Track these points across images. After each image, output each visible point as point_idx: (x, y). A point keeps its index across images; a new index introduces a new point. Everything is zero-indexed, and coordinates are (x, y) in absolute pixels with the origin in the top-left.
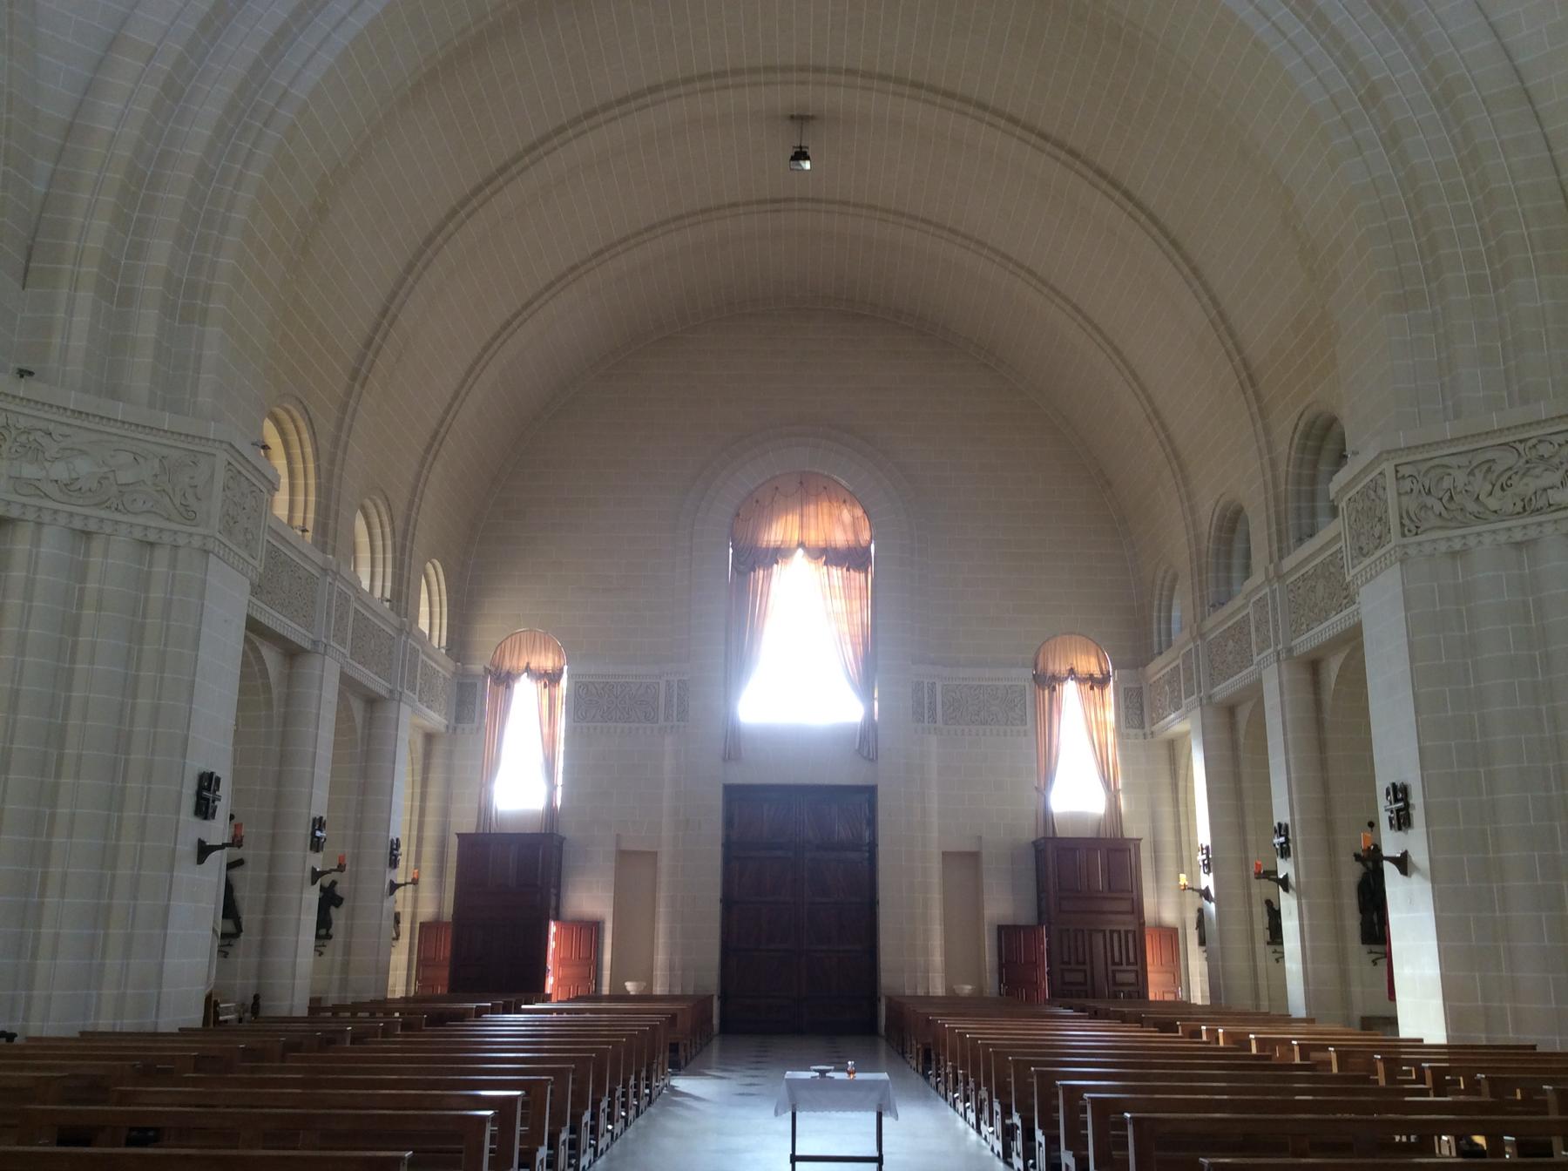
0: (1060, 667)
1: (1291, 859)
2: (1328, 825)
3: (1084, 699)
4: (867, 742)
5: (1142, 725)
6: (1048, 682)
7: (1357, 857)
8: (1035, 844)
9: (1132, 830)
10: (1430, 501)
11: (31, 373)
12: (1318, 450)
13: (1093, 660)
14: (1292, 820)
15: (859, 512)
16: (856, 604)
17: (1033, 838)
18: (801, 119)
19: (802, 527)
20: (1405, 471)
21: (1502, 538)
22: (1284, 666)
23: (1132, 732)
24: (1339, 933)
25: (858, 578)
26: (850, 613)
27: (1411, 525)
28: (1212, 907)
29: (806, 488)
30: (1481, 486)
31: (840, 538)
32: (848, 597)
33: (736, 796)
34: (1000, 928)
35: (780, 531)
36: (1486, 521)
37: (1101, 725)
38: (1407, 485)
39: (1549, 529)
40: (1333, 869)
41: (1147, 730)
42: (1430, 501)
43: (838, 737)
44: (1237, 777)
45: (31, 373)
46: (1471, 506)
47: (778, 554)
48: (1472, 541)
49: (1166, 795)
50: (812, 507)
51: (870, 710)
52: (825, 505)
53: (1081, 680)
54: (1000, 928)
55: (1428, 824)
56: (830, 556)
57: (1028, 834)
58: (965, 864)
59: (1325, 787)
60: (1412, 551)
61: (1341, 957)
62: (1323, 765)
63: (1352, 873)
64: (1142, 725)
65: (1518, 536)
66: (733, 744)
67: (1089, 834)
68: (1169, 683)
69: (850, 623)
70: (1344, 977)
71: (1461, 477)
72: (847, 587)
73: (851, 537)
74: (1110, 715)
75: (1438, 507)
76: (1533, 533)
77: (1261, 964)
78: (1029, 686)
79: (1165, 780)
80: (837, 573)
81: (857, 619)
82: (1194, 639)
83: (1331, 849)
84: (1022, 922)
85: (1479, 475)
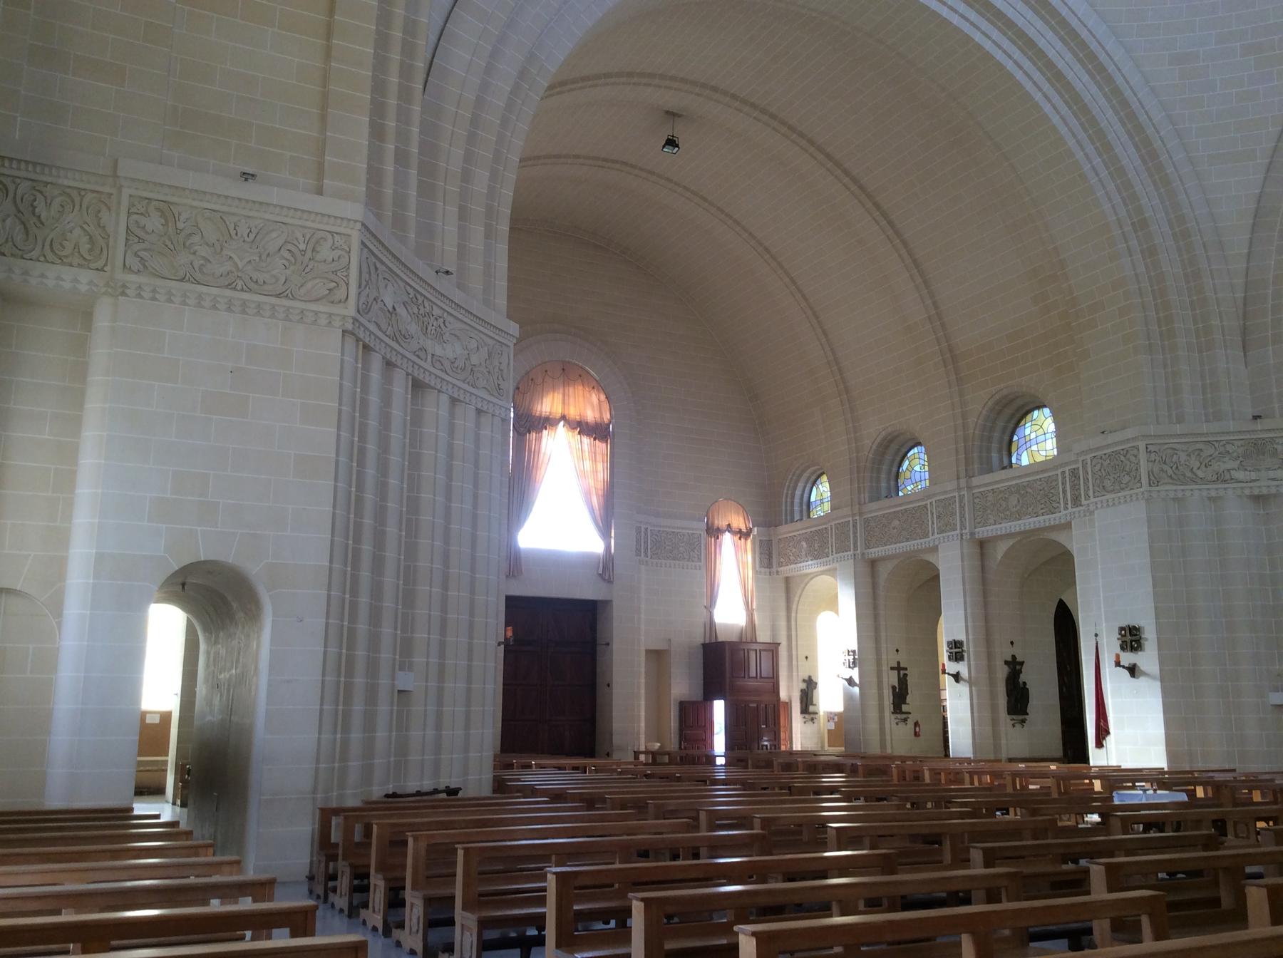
0: (721, 522)
1: (966, 662)
2: (988, 641)
3: (736, 547)
4: (606, 568)
5: (770, 565)
6: (714, 532)
7: (1006, 662)
8: (705, 646)
9: (763, 636)
10: (1166, 468)
11: (1260, 417)
12: (999, 413)
13: (741, 519)
14: (968, 639)
15: (603, 397)
16: (600, 466)
17: (702, 641)
18: (672, 115)
19: (564, 403)
20: (1151, 448)
21: (1205, 494)
22: (965, 543)
23: (763, 570)
24: (994, 709)
25: (601, 447)
26: (595, 472)
27: (1154, 481)
28: (856, 690)
29: (568, 374)
30: (1195, 463)
31: (590, 415)
32: (595, 461)
33: (515, 606)
34: (681, 703)
35: (549, 404)
36: (1196, 483)
37: (744, 564)
38: (1153, 456)
39: (1230, 492)
40: (991, 670)
41: (774, 570)
42: (1166, 468)
43: (584, 561)
44: (875, 608)
45: (1260, 417)
46: (1189, 474)
47: (547, 422)
48: (1188, 494)
49: (783, 614)
50: (571, 389)
51: (608, 548)
52: (581, 388)
53: (733, 533)
54: (681, 703)
55: (1160, 645)
56: (582, 427)
57: (699, 638)
58: (658, 657)
59: (987, 619)
60: (1154, 495)
61: (995, 722)
62: (986, 605)
63: (1002, 672)
64: (770, 565)
65: (1213, 494)
66: (515, 563)
67: (734, 638)
68: (807, 540)
69: (596, 480)
70: (996, 735)
71: (1183, 457)
72: (594, 454)
73: (597, 415)
74: (749, 557)
75: (1170, 472)
76: (1221, 493)
77: (887, 726)
78: (704, 534)
79: (783, 604)
80: (586, 441)
81: (600, 476)
82: (853, 515)
83: (990, 656)
84: (694, 699)
85: (1193, 457)
